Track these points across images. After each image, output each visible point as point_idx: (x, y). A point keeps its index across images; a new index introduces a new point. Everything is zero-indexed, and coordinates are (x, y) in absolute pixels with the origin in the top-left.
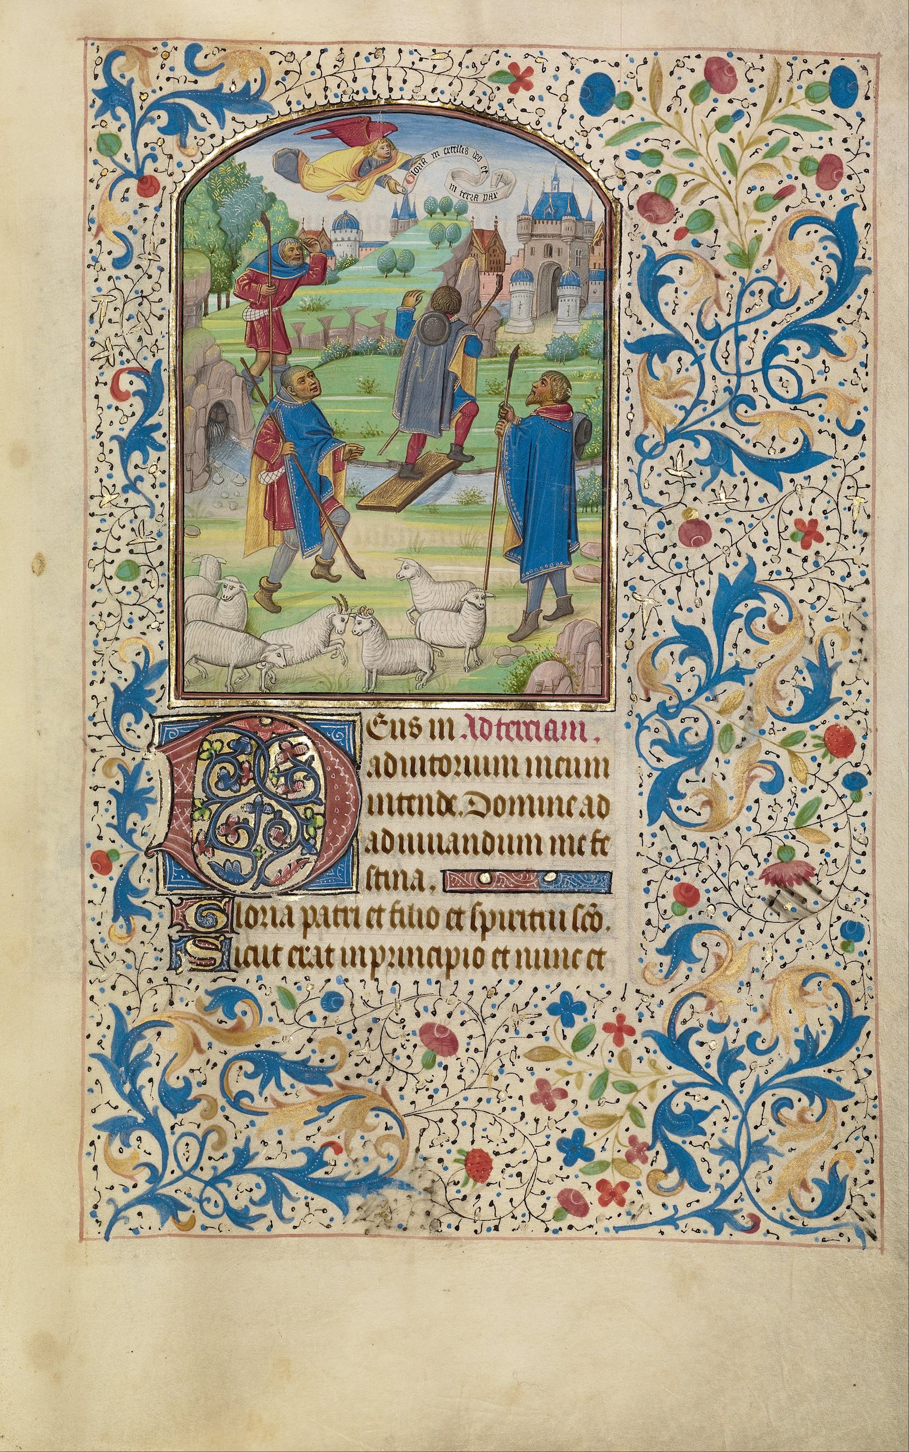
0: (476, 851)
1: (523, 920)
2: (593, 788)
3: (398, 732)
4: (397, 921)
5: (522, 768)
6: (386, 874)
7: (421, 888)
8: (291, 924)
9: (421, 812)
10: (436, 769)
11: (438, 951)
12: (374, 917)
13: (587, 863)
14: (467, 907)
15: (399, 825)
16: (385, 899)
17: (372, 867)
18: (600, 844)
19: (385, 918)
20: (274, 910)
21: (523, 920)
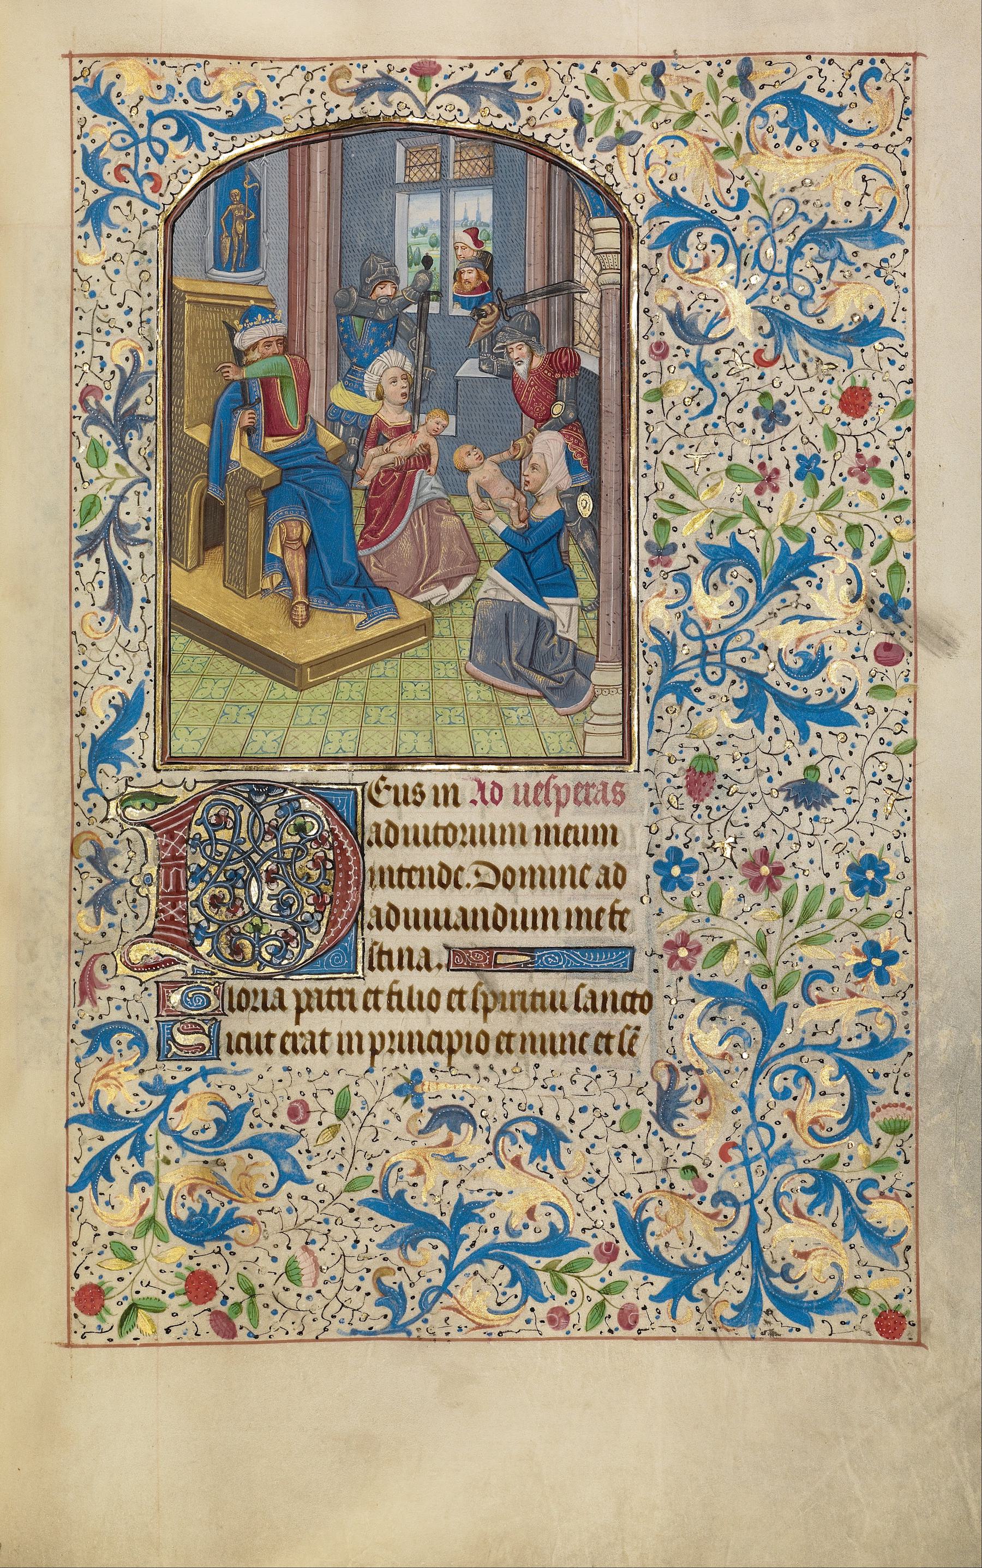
0: (486, 927)
1: (523, 1001)
2: (606, 855)
3: (402, 798)
4: (394, 1003)
5: (531, 836)
6: (389, 953)
7: (428, 968)
8: (282, 1007)
9: (422, 885)
10: (441, 839)
11: (439, 1035)
12: (455, 999)
13: (608, 937)
14: (469, 988)
15: (406, 899)
16: (381, 980)
17: (375, 943)
18: (618, 918)
19: (383, 1000)
20: (265, 992)
21: (523, 1001)
